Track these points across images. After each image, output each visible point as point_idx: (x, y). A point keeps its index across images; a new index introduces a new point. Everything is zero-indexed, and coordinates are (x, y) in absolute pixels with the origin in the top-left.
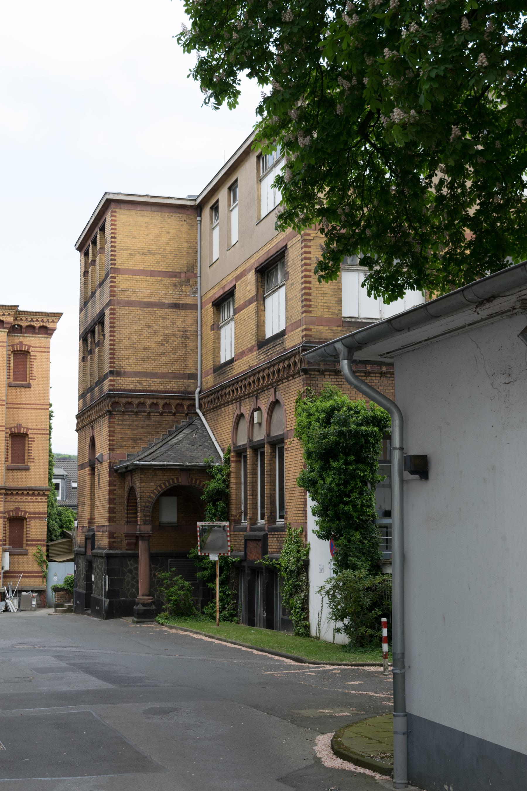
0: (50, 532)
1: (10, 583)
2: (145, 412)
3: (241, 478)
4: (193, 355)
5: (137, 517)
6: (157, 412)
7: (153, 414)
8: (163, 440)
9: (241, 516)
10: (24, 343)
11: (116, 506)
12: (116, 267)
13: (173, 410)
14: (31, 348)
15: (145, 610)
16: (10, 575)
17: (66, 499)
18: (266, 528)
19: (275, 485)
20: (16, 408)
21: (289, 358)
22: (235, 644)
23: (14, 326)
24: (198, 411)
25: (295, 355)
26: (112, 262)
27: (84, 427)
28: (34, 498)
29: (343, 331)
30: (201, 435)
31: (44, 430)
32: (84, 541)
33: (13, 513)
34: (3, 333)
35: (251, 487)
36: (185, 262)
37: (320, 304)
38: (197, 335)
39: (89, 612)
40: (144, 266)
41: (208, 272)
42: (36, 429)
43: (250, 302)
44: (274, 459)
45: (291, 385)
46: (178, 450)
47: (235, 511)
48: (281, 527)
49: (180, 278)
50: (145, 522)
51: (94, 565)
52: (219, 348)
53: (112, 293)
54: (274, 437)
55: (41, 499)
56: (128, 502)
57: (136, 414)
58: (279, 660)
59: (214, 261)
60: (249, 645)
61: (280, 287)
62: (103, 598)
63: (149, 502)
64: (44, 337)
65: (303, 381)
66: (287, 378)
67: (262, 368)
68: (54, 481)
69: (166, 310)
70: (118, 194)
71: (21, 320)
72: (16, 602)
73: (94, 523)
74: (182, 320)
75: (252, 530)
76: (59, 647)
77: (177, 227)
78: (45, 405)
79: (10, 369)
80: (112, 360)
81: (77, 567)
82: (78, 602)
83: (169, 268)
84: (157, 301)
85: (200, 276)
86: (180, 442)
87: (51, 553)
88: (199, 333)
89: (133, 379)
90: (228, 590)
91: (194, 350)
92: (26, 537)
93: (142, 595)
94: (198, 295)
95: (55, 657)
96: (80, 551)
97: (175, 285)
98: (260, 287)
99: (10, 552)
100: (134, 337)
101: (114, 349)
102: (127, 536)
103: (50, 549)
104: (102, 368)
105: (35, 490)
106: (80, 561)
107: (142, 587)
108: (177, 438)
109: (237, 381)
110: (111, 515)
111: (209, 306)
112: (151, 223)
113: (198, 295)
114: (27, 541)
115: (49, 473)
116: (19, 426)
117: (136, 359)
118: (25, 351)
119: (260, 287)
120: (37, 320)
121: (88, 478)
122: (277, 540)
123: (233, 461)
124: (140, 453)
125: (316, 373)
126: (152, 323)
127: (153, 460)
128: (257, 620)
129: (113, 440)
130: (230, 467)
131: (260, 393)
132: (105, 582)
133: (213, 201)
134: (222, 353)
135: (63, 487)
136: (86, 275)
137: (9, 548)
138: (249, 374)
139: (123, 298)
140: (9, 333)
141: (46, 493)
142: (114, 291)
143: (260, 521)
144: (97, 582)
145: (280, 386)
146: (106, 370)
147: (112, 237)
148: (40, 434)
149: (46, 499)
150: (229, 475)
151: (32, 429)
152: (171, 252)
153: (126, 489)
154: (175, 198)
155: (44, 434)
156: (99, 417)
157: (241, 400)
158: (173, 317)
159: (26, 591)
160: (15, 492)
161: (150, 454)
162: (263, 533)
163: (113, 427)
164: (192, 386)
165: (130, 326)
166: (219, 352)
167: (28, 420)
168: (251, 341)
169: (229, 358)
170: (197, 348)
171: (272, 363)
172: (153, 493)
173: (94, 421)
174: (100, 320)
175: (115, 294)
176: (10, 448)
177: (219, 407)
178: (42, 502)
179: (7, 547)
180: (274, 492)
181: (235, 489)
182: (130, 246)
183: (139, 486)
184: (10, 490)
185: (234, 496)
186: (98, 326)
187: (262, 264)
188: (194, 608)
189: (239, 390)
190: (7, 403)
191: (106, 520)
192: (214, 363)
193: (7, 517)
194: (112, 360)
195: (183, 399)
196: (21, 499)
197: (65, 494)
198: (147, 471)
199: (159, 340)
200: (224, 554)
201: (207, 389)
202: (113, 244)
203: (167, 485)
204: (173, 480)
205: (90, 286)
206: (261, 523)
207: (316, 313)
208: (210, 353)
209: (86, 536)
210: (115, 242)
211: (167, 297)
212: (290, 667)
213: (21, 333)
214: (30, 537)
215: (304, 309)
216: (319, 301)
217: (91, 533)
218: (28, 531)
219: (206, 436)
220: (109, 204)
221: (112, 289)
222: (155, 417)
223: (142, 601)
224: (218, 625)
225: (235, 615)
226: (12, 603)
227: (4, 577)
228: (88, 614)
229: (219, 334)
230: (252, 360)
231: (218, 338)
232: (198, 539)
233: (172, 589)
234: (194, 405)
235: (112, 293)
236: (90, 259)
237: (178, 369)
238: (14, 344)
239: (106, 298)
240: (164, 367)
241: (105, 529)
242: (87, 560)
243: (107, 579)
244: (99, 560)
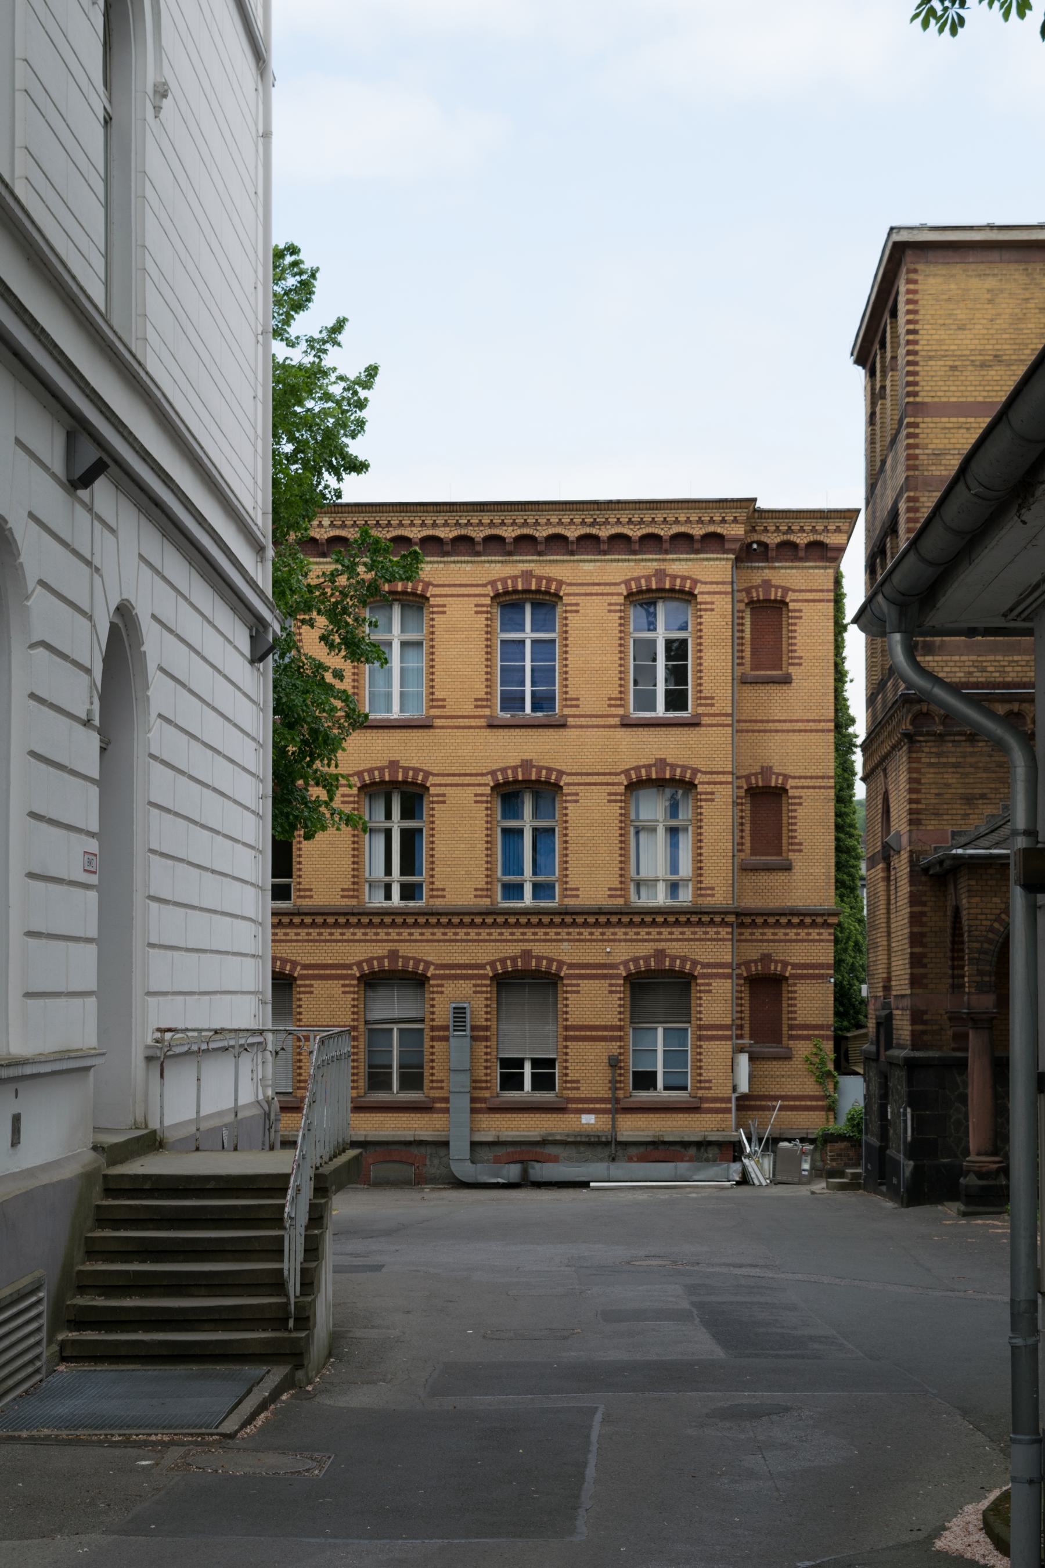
10: (774, 582)
12: (918, 399)
14: (790, 593)
16: (753, 1103)
20: (759, 731)
28: (803, 933)
31: (823, 777)
33: (756, 966)
34: (724, 563)
39: (884, 1188)
42: (806, 778)
53: (911, 462)
55: (819, 934)
62: (901, 1157)
71: (766, 530)
72: (767, 1163)
89: (964, 658)
105: (805, 915)
112: (1002, 291)
114: (791, 1027)
116: (766, 771)
118: (775, 601)
120: (802, 530)
127: (997, 845)
129: (917, 801)
132: (905, 1121)
140: (738, 560)
142: (915, 457)
148: (814, 787)
149: (830, 934)
151: (794, 778)
159: (789, 1140)
160: (759, 920)
163: (918, 770)
176: (747, 821)
179: (746, 1041)
182: (952, 347)
183: (967, 906)
193: (745, 975)
213: (767, 561)
214: (795, 1019)
221: (911, 451)
226: (759, 1167)
227: (739, 1108)
235: (911, 462)
243: (909, 1116)
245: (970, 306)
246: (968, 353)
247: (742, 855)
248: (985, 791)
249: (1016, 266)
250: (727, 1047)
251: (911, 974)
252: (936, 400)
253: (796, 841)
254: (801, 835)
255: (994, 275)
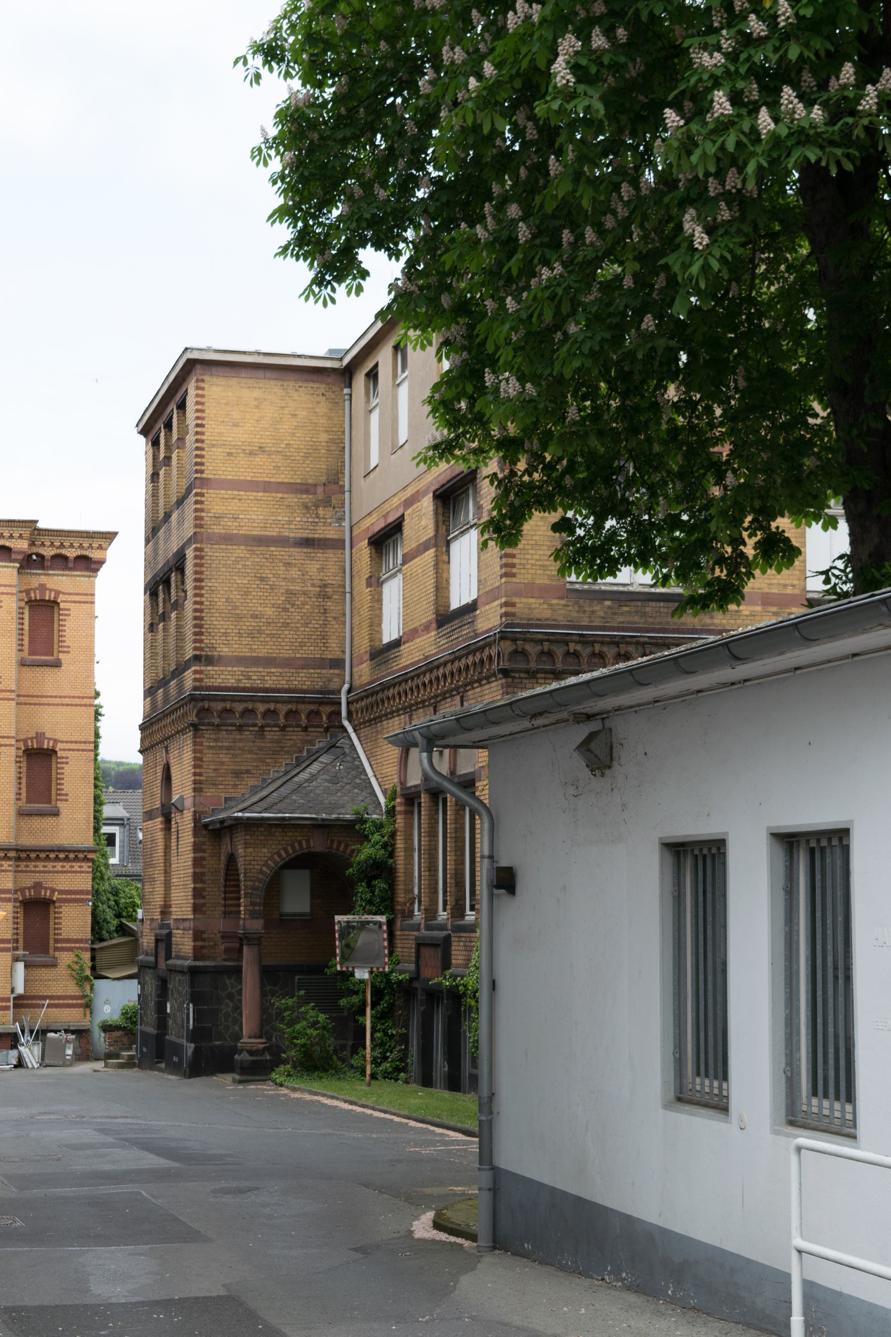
0: (97, 924)
1: (27, 1016)
2: (255, 725)
3: (413, 840)
4: (337, 626)
5: (239, 905)
6: (275, 726)
7: (269, 729)
8: (286, 773)
9: (412, 904)
10: (48, 586)
11: (206, 886)
12: (204, 476)
13: (304, 721)
14: (61, 595)
15: (253, 1062)
16: (25, 1002)
17: (128, 863)
18: (449, 927)
19: (463, 855)
20: (35, 704)
21: (482, 649)
22: (385, 1112)
23: (30, 555)
24: (346, 723)
25: (489, 645)
26: (198, 467)
27: (152, 746)
28: (67, 865)
29: (568, 606)
30: (349, 765)
31: (85, 742)
32: (153, 945)
34: (10, 569)
35: (426, 856)
36: (324, 467)
37: (530, 562)
38: (345, 593)
39: (163, 1065)
40: (252, 474)
41: (362, 485)
42: (71, 742)
43: (424, 547)
44: (461, 812)
45: (485, 692)
46: (309, 792)
47: (403, 895)
48: (471, 925)
49: (315, 493)
50: (253, 915)
51: (170, 986)
52: (379, 617)
53: (198, 522)
54: (460, 776)
55: (80, 867)
56: (226, 880)
57: (240, 728)
58: (442, 1134)
59: (372, 468)
60: (406, 1113)
61: (471, 527)
63: (260, 881)
64: (84, 576)
65: (502, 688)
66: (479, 681)
67: (442, 660)
68: (105, 829)
69: (291, 549)
70: (208, 350)
71: (43, 545)
72: (37, 1050)
73: (170, 913)
74: (318, 566)
75: (428, 928)
76: (106, 1117)
77: (310, 405)
78: (86, 697)
79: (22, 634)
80: (198, 637)
81: (142, 989)
82: (144, 1049)
83: (296, 477)
84: (275, 534)
85: (350, 491)
86: (313, 777)
87: (98, 966)
88: (348, 589)
89: (235, 669)
90: (391, 1028)
91: (340, 618)
92: (55, 934)
93: (248, 1036)
94: (346, 524)
95: (99, 1130)
96: (147, 962)
97: (306, 507)
98: (440, 523)
99: (25, 962)
100: (236, 596)
101: (201, 618)
102: (225, 936)
103: (98, 956)
104: (182, 647)
105: (69, 851)
106: (147, 978)
107: (248, 1023)
108: (308, 770)
109: (405, 678)
110: (198, 901)
111: (363, 543)
113: (346, 524)
114: (57, 941)
115: (95, 818)
116: (40, 736)
117: (240, 635)
118: (49, 601)
119: (440, 523)
120: (72, 546)
121: (160, 836)
122: (465, 946)
123: (400, 812)
124: (247, 796)
125: (523, 675)
126: (267, 573)
127: (266, 810)
128: (436, 1077)
129: (200, 774)
130: (395, 821)
131: (439, 701)
132: (188, 1014)
133: (369, 365)
134: (385, 626)
135: (122, 841)
136: (155, 480)
137: (24, 955)
138: (423, 669)
139: (217, 530)
140: (20, 570)
141: (90, 856)
142: (202, 518)
143: (442, 913)
144: (175, 1015)
145: (470, 693)
146: (189, 653)
147: (197, 425)
148: (78, 750)
149: (89, 867)
150: (393, 835)
151: (63, 742)
152: (299, 448)
153: (223, 858)
154: (305, 357)
155: (86, 750)
156: (178, 732)
157: (411, 711)
158: (303, 562)
159: (55, 1032)
160: (33, 855)
161: (262, 800)
162: (442, 934)
163: (200, 752)
164: (335, 680)
165: (229, 577)
166: (380, 625)
167: (57, 725)
168: (427, 614)
169: (395, 636)
170: (344, 615)
171: (457, 654)
172: (266, 865)
173: (169, 738)
174: (178, 564)
175: (203, 522)
176: (24, 775)
177: (379, 719)
178: (83, 872)
179: (21, 952)
180: (462, 867)
181: (402, 858)
182: (229, 439)
184: (25, 851)
185: (402, 871)
186: (176, 575)
187: (444, 485)
188: (335, 1057)
189: (409, 693)
190: (18, 696)
191: (189, 909)
192: (372, 643)
193: (21, 899)
194: (198, 637)
195: (321, 702)
196: (44, 866)
197: (126, 854)
198: (255, 829)
199: (279, 602)
200: (378, 969)
201: (362, 686)
202: (199, 437)
203: (291, 851)
204: (300, 843)
205: (161, 502)
206: (443, 915)
207: (523, 577)
208: (366, 624)
209: (156, 935)
210: (203, 434)
211: (294, 527)
212: (458, 1142)
213: (43, 569)
214: (60, 934)
215: (503, 570)
216: (529, 557)
217: (165, 932)
218: (58, 924)
219: (358, 768)
220: (191, 368)
221: (198, 514)
222: (272, 735)
223: (248, 1047)
224: (369, 1085)
225: (404, 1070)
226: (31, 1052)
228: (160, 1070)
229: (380, 594)
230: (426, 647)
231: (378, 600)
232: (337, 943)
233: (298, 1027)
234: (339, 713)
235: (198, 522)
236: (162, 456)
237: (311, 651)
238: (31, 589)
239: (189, 531)
240: (288, 648)
241: (187, 924)
242: (159, 977)
243: (191, 1010)
244: (179, 977)
245: (242, 409)
246: (240, 443)
247: (20, 803)
248: (249, 768)
249: (275, 382)
250: (8, 956)
251: (194, 903)
252: (217, 477)
253: (63, 792)
254: (67, 787)
255: (260, 388)
